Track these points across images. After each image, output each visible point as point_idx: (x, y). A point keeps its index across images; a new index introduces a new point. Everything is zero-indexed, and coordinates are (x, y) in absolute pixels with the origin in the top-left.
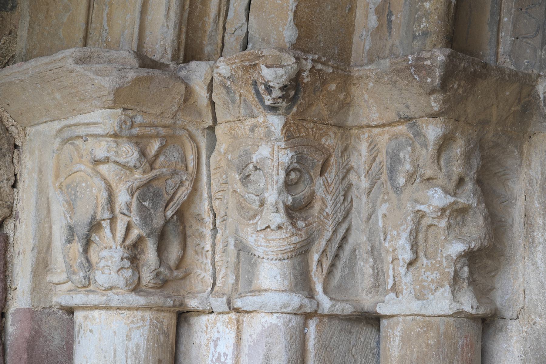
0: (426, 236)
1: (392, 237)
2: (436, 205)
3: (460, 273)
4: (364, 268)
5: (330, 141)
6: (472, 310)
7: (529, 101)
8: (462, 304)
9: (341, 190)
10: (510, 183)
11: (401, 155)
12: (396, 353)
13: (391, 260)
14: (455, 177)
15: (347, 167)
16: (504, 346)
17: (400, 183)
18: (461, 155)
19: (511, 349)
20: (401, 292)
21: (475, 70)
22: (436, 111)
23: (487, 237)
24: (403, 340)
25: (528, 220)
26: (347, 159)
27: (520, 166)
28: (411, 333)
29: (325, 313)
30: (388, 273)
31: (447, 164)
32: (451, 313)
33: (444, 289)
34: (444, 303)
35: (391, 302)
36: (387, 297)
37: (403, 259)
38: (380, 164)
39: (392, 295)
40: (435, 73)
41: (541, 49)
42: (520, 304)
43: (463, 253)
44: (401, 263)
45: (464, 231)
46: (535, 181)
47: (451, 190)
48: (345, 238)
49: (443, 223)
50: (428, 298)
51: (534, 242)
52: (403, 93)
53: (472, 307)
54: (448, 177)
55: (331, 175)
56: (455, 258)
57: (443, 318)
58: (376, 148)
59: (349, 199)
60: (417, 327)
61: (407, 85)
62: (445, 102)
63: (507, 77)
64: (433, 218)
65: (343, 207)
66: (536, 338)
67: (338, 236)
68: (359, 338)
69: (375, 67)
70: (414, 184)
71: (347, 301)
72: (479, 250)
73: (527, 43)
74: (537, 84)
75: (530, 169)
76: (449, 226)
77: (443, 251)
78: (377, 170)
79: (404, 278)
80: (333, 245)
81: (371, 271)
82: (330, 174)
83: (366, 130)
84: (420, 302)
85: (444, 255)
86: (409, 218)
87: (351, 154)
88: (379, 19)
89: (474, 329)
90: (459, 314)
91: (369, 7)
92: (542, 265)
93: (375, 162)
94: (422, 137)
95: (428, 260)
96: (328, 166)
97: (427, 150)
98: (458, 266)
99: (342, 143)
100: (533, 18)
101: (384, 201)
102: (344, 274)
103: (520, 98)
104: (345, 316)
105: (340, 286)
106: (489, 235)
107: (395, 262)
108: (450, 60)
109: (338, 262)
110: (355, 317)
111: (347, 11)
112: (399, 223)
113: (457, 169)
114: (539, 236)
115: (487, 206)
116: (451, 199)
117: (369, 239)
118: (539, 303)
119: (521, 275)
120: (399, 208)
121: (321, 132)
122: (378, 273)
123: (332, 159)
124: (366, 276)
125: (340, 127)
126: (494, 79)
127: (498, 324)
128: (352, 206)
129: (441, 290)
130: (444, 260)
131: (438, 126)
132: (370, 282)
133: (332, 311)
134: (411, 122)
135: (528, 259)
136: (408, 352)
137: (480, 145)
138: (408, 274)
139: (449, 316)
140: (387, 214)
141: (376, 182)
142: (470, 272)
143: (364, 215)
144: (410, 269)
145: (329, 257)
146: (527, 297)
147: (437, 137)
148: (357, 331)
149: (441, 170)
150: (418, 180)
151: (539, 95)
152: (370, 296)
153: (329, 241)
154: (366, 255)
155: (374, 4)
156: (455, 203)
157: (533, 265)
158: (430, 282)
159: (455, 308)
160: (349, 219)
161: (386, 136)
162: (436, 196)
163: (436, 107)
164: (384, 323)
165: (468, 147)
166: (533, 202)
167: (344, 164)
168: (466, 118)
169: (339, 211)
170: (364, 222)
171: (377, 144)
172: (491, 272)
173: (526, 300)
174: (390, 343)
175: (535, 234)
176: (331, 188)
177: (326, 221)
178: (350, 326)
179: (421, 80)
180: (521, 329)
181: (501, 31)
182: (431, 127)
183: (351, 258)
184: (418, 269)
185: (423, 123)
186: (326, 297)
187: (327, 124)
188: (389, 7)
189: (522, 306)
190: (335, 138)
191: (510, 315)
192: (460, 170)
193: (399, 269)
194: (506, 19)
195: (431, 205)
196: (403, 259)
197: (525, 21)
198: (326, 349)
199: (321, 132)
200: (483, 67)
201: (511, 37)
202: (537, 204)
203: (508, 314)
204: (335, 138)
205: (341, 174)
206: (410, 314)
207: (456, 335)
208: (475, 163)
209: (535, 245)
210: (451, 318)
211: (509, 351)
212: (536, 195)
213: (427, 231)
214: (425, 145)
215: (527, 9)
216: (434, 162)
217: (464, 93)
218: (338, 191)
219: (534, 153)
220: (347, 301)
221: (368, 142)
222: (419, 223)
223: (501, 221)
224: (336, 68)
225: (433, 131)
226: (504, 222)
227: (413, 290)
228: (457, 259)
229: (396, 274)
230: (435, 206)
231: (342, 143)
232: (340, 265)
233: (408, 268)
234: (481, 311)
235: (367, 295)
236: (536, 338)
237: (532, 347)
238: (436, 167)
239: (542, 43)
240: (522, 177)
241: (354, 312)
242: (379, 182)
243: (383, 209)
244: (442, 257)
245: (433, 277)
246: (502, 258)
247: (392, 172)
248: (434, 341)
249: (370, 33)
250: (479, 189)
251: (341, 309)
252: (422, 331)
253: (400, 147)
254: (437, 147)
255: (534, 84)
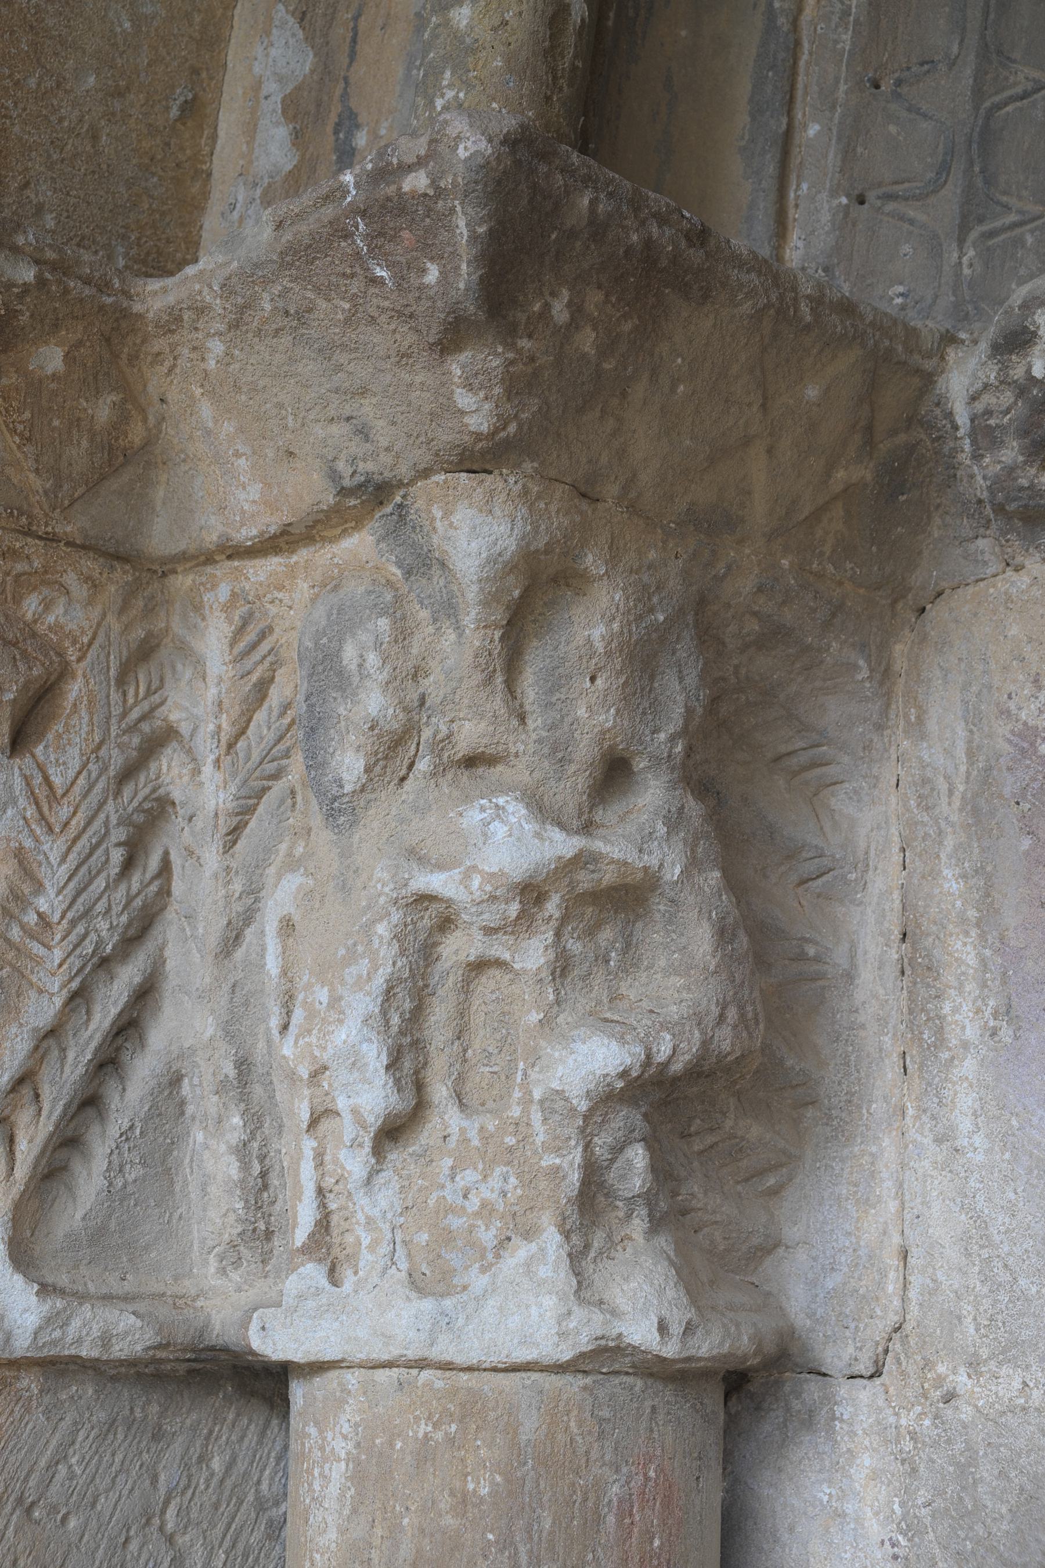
0: (462, 1012)
1: (311, 1014)
2: (495, 869)
3: (611, 1177)
4: (207, 1155)
5: (68, 611)
6: (663, 1342)
7: (911, 448)
8: (614, 1313)
9: (114, 820)
10: (839, 801)
11: (349, 653)
12: (332, 1535)
13: (305, 1116)
14: (585, 750)
15: (145, 727)
16: (824, 1492)
17: (346, 776)
18: (608, 654)
19: (849, 1508)
20: (353, 1259)
21: (648, 243)
22: (478, 436)
23: (732, 1014)
24: (358, 1476)
25: (915, 950)
26: (149, 693)
27: (880, 727)
28: (392, 1445)
29: (18, 1353)
30: (297, 1174)
31: (551, 691)
32: (567, 1356)
33: (533, 1247)
34: (534, 1311)
35: (311, 1304)
36: (292, 1284)
37: (355, 1111)
38: (282, 714)
39: (312, 1272)
40: (451, 229)
41: (961, 242)
42: (885, 1309)
43: (620, 1084)
44: (348, 1129)
45: (631, 989)
46: (943, 786)
47: (571, 808)
48: (129, 1028)
49: (533, 955)
50: (465, 1288)
51: (940, 1040)
52: (339, 368)
53: (663, 1328)
54: (555, 750)
55: (66, 752)
56: (583, 1106)
57: (535, 1376)
58: (265, 647)
59: (154, 863)
60: (417, 1419)
61: (347, 321)
62: (516, 386)
63: (804, 308)
64: (489, 931)
65: (120, 895)
66: (958, 1464)
67: (97, 1017)
68: (201, 1459)
69: (221, 259)
70: (408, 785)
71: (128, 1298)
72: (696, 1072)
73: (902, 218)
74: (941, 370)
75: (923, 737)
76: (562, 967)
77: (534, 1075)
78: (271, 736)
79: (362, 1200)
80: (71, 1055)
81: (232, 1169)
82: (61, 749)
83: (223, 568)
84: (427, 1305)
85: (537, 1095)
86: (382, 929)
87: (168, 675)
88: (298, 138)
89: (678, 1430)
90: (604, 1358)
91: (264, 92)
92: (978, 1140)
93: (266, 705)
94: (436, 571)
95: (469, 1116)
96: (53, 717)
97: (459, 629)
98: (602, 1142)
99: (127, 628)
100: (925, 116)
101: (292, 864)
102: (119, 1183)
103: (869, 430)
104: (121, 1362)
105: (97, 1235)
106: (741, 1008)
107: (325, 1125)
108: (518, 163)
109: (95, 1129)
110: (182, 1368)
111: (174, 113)
112: (342, 952)
113: (593, 714)
114: (964, 1014)
115: (735, 884)
116: (563, 845)
117: (230, 1031)
118: (967, 1308)
119: (889, 1184)
120: (344, 888)
121: (20, 567)
122: (264, 1175)
123: (74, 689)
124: (213, 1189)
125: (119, 556)
126: (747, 307)
127: (798, 1395)
128: (165, 892)
129: (522, 1251)
130: (536, 1117)
131: (498, 513)
132: (232, 1218)
133: (54, 1343)
134: (388, 509)
135: (917, 1118)
136: (379, 1531)
137: (701, 616)
138: (380, 1179)
139: (559, 1368)
140: (296, 918)
141: (265, 790)
142: (661, 1171)
143: (211, 927)
144: (392, 1156)
145: (46, 1106)
146: (916, 1281)
147: (491, 560)
148: (194, 1429)
149: (522, 719)
150: (423, 765)
151: (950, 415)
152: (235, 1276)
153: (52, 1035)
154: (215, 1098)
155: (281, 79)
156: (581, 860)
157: (939, 1141)
158: (477, 1214)
159: (585, 1330)
160: (150, 945)
161: (303, 588)
162: (499, 830)
163: (476, 412)
164: (298, 1392)
165: (639, 618)
166: (934, 874)
167: (135, 714)
168: (625, 488)
169: (100, 907)
170: (210, 958)
171: (270, 629)
172: (762, 1173)
173: (912, 1294)
174: (310, 1485)
175: (947, 1008)
176: (65, 812)
177: (37, 949)
178: (154, 1409)
179: (400, 279)
180: (892, 1420)
181: (793, 178)
182: (464, 515)
183: (154, 1113)
184: (426, 1157)
185: (430, 501)
186: (18, 1279)
187: (51, 539)
188: (345, 96)
189: (893, 1319)
190: (90, 602)
191: (846, 1357)
192: (607, 718)
193: (343, 1154)
194: (813, 130)
195: (474, 868)
196: (355, 1111)
197: (893, 129)
198: (29, 1511)
199: (20, 567)
200: (688, 237)
201: (834, 193)
202: (950, 882)
203: (837, 1355)
204: (90, 602)
205: (115, 752)
206: (385, 1357)
207: (594, 1455)
208: (678, 693)
209: (945, 1055)
210: (569, 1378)
211: (843, 1515)
212: (949, 842)
213: (466, 987)
214: (447, 609)
215: (899, 83)
216: (489, 680)
217: (605, 350)
218: (98, 824)
219: (938, 673)
220: (128, 1298)
221: (229, 620)
222: (428, 953)
223: (801, 957)
224: (54, 266)
225: (475, 531)
226: (817, 959)
227: (401, 1252)
228: (591, 1110)
229: (329, 1182)
230: (493, 875)
231: (127, 628)
232: (102, 1144)
233: (378, 1152)
234: (707, 1346)
235: (223, 1272)
236: (958, 1464)
237: (940, 1503)
238: (498, 704)
239: (964, 217)
240: (888, 773)
241: (159, 1347)
242: (278, 788)
243: (283, 896)
244: (527, 1101)
245: (489, 1191)
246: (810, 1112)
247: (314, 727)
248: (493, 1483)
249: (259, 191)
250: (694, 808)
251: (96, 1333)
252: (439, 1436)
253: (343, 622)
254: (499, 615)
255: (928, 365)
